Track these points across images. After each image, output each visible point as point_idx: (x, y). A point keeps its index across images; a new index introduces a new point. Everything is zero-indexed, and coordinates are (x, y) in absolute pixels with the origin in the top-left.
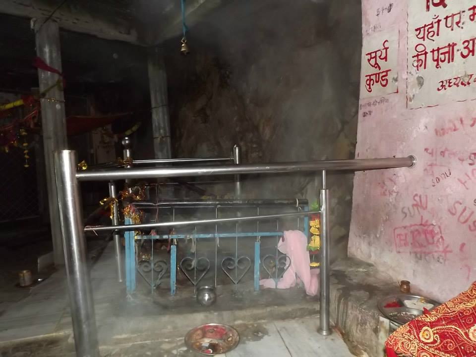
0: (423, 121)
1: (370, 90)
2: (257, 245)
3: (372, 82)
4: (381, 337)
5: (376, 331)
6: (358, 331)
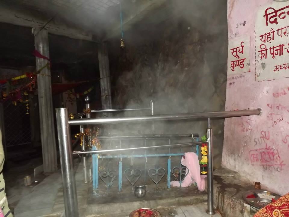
0: (266, 89)
1: (233, 70)
3: (234, 65)
6: (231, 212)
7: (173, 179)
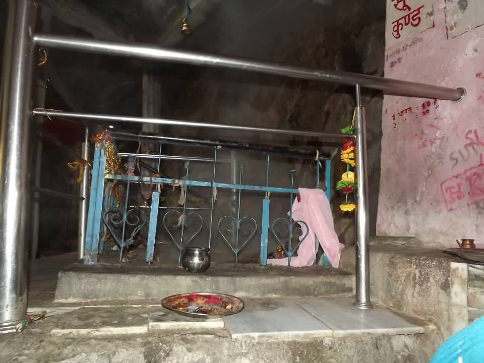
0: (470, 46)
1: (398, 36)
2: (266, 203)
3: (400, 27)
4: (455, 293)
5: (446, 286)
6: (416, 295)
7: (270, 255)
